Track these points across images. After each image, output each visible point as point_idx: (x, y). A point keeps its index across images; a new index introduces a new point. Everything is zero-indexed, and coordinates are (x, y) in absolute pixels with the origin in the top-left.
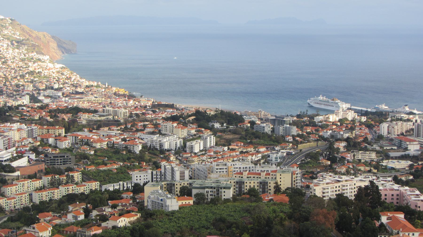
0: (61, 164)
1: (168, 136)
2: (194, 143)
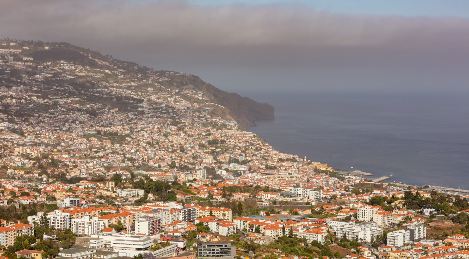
0: (218, 256)
1: (363, 224)
2: (396, 234)
